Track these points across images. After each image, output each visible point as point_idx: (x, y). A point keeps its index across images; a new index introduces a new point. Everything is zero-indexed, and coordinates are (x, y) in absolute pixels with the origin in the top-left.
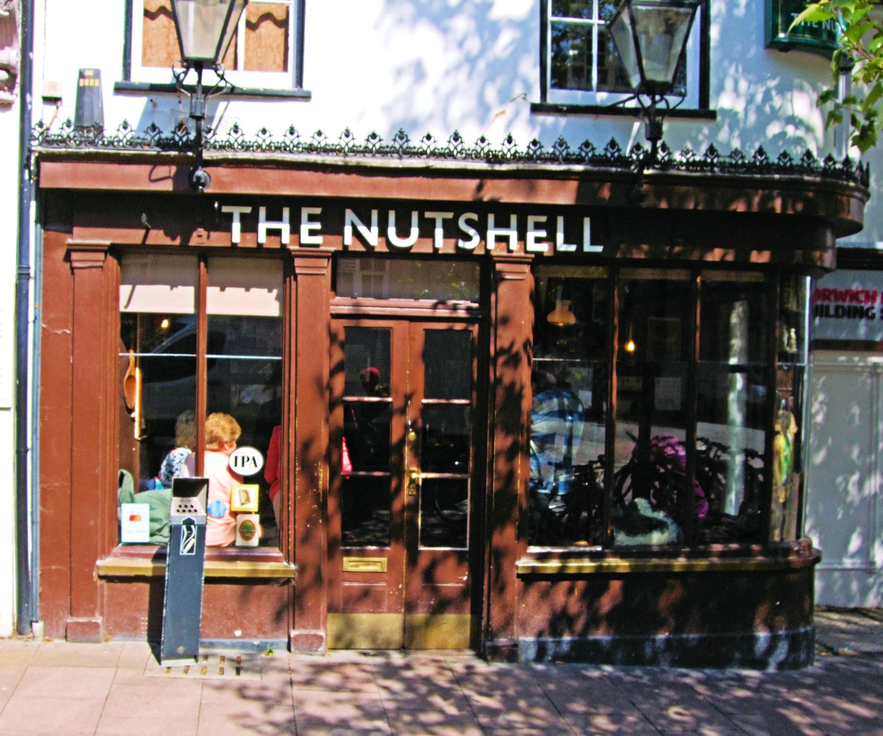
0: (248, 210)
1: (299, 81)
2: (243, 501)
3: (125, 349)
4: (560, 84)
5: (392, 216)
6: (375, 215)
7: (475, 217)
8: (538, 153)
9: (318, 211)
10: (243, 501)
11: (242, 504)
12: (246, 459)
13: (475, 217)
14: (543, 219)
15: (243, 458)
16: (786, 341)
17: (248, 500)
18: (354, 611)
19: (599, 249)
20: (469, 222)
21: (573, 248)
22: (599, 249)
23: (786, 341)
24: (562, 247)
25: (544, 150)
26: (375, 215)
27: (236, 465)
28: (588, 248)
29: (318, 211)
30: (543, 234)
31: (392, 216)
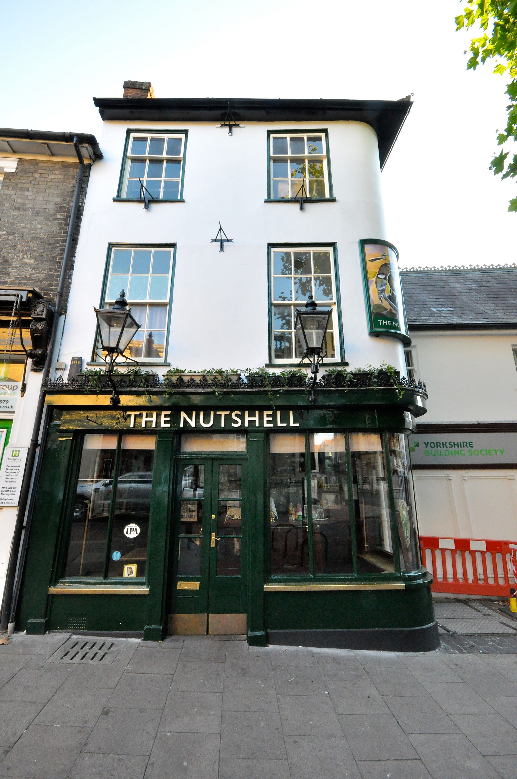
0: (138, 413)
1: (166, 359)
2: (129, 573)
3: (166, 307)
4: (277, 356)
5: (202, 414)
6: (194, 413)
7: (239, 413)
8: (193, 383)
9: (169, 413)
10: (129, 573)
11: (129, 575)
12: (132, 530)
13: (239, 413)
14: (271, 413)
15: (131, 529)
16: (396, 465)
17: (132, 572)
18: (145, 458)
19: (297, 425)
20: (236, 415)
21: (285, 425)
22: (297, 425)
23: (396, 465)
24: (279, 424)
25: (64, 382)
26: (194, 413)
27: (127, 533)
28: (292, 424)
29: (169, 413)
30: (271, 419)
31: (202, 414)
